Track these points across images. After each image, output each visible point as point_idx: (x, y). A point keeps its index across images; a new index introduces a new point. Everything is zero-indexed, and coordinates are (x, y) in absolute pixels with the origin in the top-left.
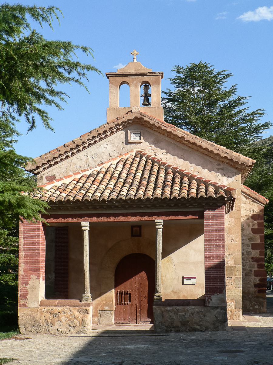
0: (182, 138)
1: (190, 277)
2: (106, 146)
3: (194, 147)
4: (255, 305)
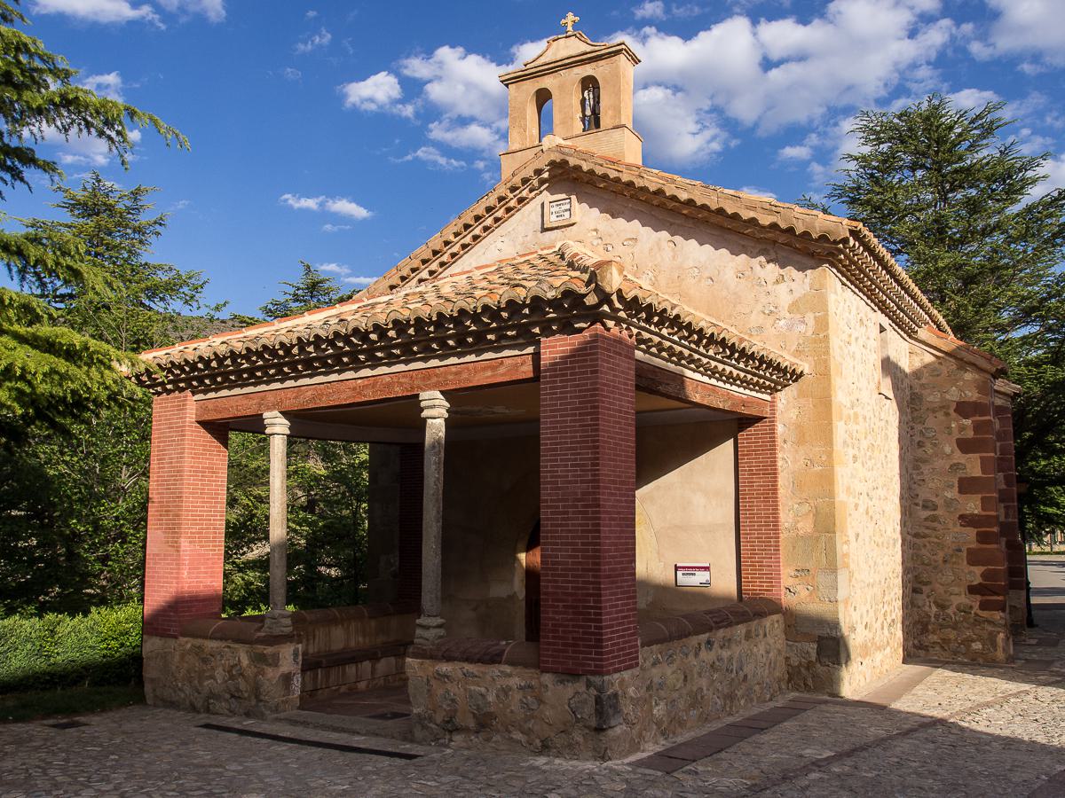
0: (660, 192)
1: (695, 567)
2: (500, 245)
3: (719, 219)
4: (973, 641)
